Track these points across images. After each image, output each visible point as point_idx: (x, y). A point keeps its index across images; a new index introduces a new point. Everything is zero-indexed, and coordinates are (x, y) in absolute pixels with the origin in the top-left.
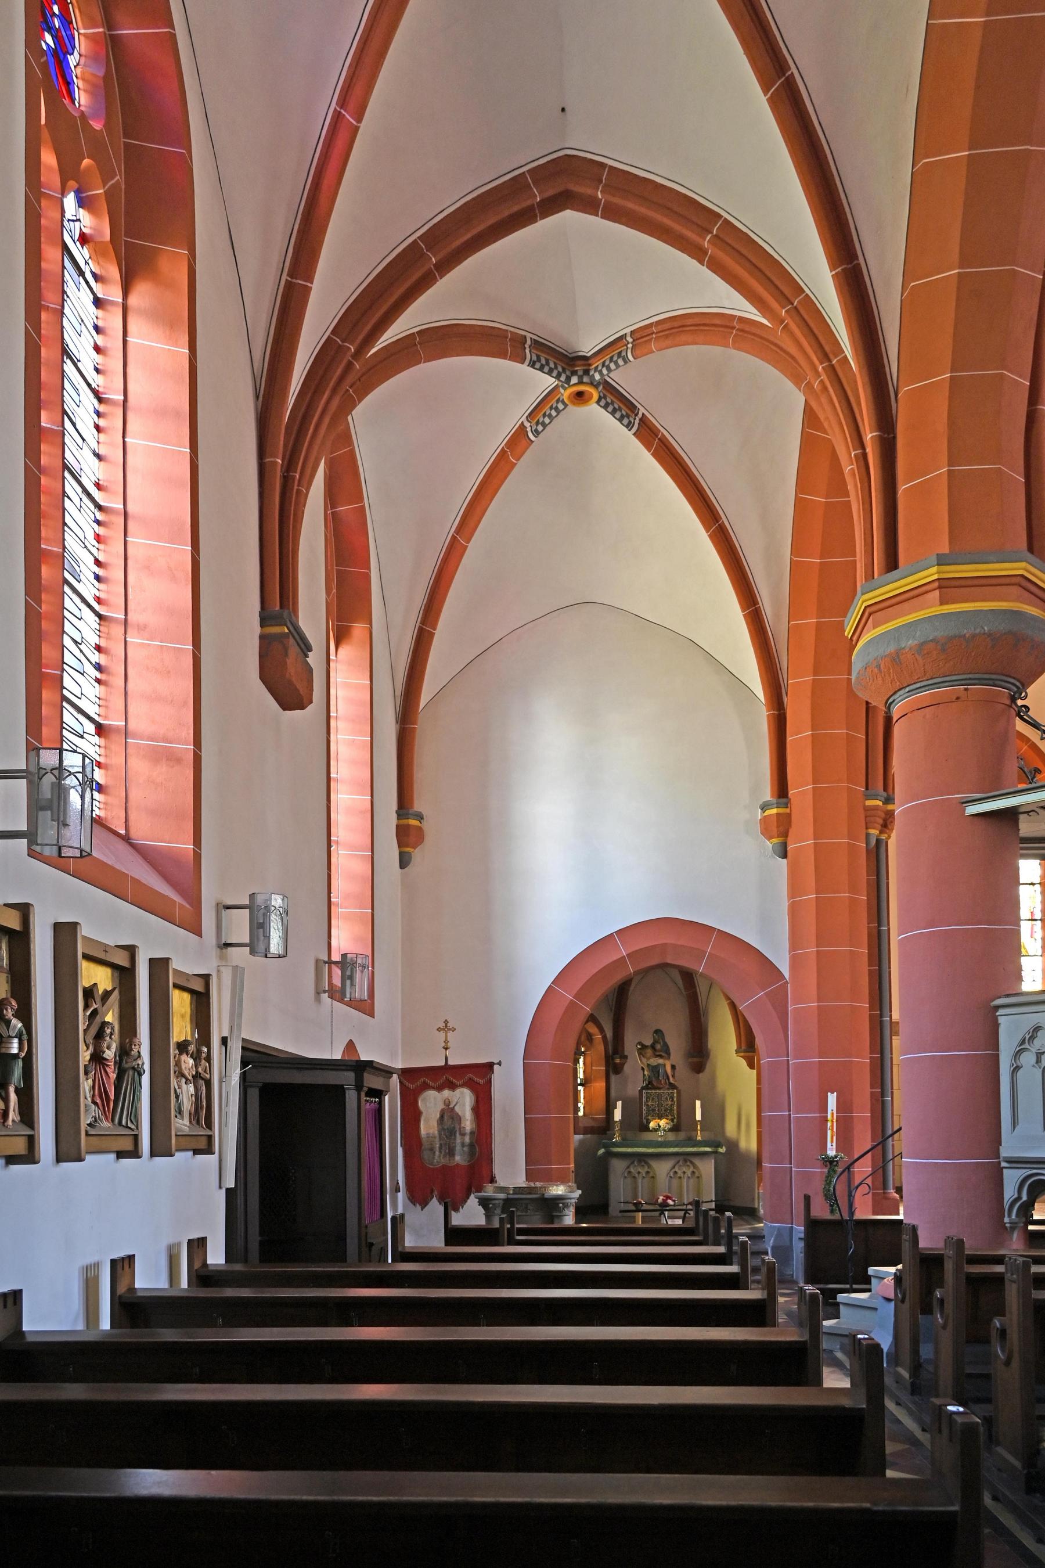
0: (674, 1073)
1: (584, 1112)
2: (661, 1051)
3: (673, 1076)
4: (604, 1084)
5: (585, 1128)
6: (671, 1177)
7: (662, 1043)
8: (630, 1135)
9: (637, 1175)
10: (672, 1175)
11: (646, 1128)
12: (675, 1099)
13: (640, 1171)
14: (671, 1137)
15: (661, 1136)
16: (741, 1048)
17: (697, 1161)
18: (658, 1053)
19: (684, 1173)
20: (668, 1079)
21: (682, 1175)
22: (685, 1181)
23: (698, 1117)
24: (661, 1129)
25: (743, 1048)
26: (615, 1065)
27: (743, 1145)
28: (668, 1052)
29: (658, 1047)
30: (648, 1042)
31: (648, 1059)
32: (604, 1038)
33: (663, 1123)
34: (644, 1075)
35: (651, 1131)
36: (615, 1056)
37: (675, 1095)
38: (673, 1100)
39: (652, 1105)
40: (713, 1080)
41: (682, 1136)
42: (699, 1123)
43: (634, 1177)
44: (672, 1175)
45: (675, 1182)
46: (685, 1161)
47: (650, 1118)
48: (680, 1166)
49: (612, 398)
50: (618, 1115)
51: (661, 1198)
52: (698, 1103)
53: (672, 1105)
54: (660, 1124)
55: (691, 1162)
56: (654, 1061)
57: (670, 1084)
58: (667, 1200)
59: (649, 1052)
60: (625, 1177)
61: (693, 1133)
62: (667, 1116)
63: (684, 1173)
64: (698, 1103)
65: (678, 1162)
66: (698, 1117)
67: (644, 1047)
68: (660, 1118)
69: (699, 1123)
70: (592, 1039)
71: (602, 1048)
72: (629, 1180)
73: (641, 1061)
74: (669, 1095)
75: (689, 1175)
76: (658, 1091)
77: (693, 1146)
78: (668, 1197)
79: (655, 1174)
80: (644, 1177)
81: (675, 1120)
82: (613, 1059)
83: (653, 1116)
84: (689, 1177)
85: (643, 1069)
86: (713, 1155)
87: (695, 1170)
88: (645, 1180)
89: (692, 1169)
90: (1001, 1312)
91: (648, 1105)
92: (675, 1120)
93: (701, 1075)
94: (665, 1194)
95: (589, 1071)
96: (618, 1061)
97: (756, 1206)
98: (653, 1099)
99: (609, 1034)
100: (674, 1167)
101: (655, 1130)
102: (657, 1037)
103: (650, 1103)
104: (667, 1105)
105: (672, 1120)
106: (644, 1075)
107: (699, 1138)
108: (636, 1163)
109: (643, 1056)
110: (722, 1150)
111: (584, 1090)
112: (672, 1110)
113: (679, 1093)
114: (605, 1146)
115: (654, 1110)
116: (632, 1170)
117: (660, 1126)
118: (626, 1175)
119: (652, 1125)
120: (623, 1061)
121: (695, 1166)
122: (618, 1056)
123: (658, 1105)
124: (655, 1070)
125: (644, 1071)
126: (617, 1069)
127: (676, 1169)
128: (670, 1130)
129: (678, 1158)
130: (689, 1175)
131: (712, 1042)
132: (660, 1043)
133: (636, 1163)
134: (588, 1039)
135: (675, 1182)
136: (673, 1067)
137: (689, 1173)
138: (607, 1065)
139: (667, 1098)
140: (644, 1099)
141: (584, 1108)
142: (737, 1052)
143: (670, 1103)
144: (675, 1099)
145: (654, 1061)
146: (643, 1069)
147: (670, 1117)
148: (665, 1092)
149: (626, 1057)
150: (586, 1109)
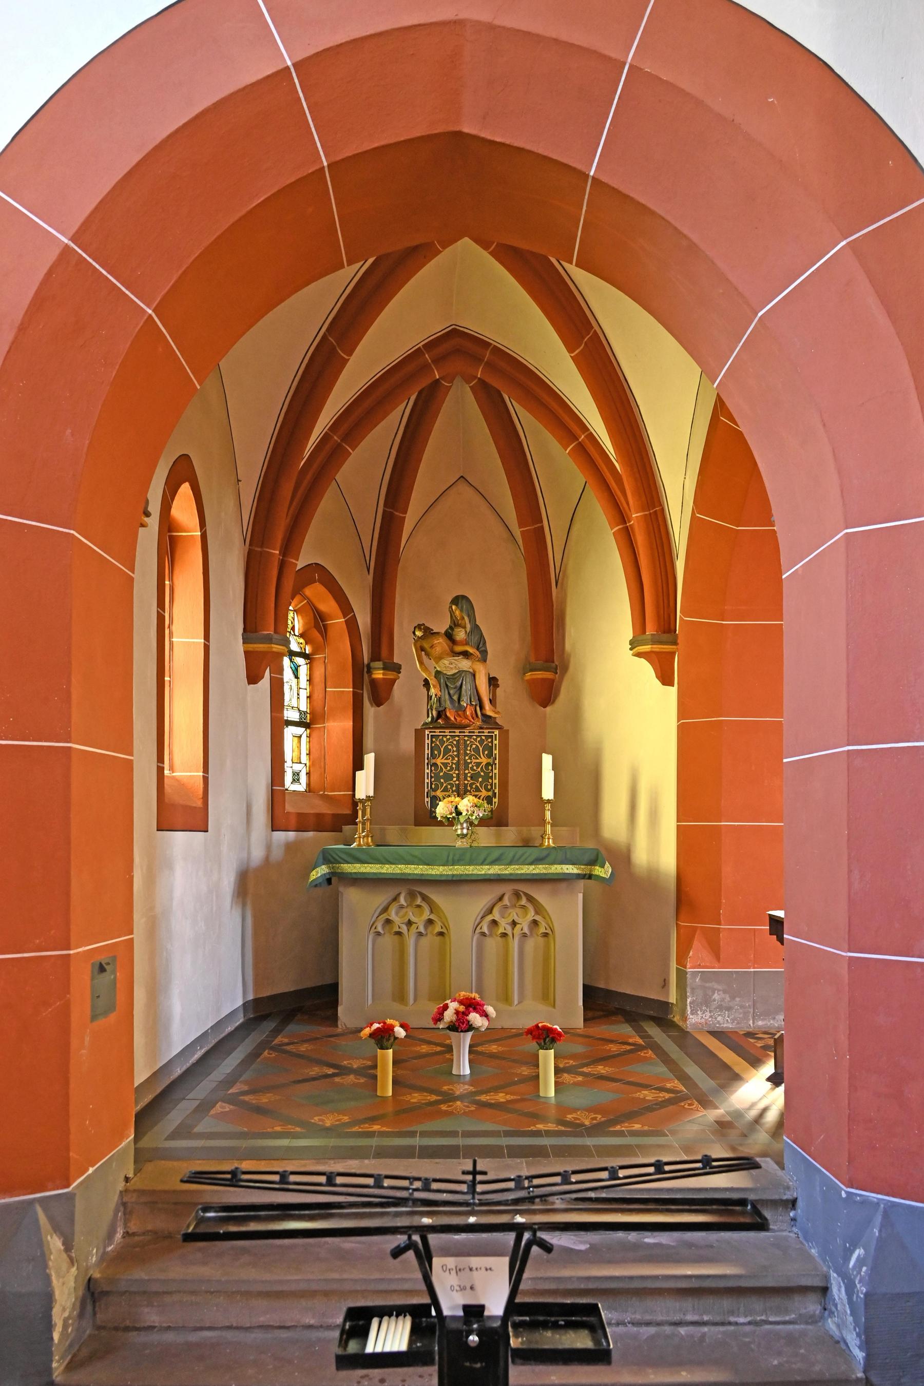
0: (494, 695)
1: (308, 785)
2: (467, 644)
3: (492, 701)
4: (349, 724)
5: (300, 815)
6: (483, 934)
7: (468, 627)
8: (393, 833)
9: (404, 929)
10: (485, 930)
11: (427, 818)
12: (496, 752)
13: (413, 919)
14: (485, 837)
15: (463, 836)
16: (644, 632)
17: (541, 895)
18: (459, 649)
19: (514, 924)
20: (482, 708)
21: (509, 930)
22: (515, 944)
23: (548, 792)
24: (462, 819)
25: (650, 630)
26: (373, 682)
27: (641, 856)
28: (481, 645)
29: (460, 635)
30: (441, 626)
31: (439, 659)
32: (352, 625)
33: (465, 804)
34: (430, 698)
35: (440, 824)
36: (374, 665)
37: (497, 742)
38: (490, 755)
39: (445, 765)
40: (575, 717)
41: (510, 835)
42: (548, 807)
43: (399, 934)
44: (485, 930)
45: (493, 944)
46: (412, 895)
47: (439, 793)
48: (506, 907)
49: (564, 1318)
50: (365, 785)
51: (453, 1006)
52: (547, 760)
53: (488, 764)
54: (461, 807)
55: (425, 898)
56: (451, 665)
57: (487, 718)
58: (466, 1014)
59: (440, 644)
60: (378, 934)
61: (535, 831)
62: (477, 790)
63: (514, 924)
64: (547, 760)
65: (396, 899)
66: (548, 792)
67: (429, 633)
68: (461, 795)
69: (548, 807)
70: (325, 626)
71: (345, 646)
72: (388, 941)
73: (421, 663)
74: (481, 742)
75: (526, 930)
76: (457, 732)
77: (537, 861)
78: (471, 1005)
79: (445, 925)
80: (420, 934)
81: (496, 800)
82: (369, 670)
83: (446, 790)
84: (524, 935)
85: (426, 684)
86: (582, 883)
87: (538, 918)
88: (424, 941)
89: (531, 915)
90: (767, 1024)
91: (435, 765)
92: (496, 800)
93: (548, 709)
94: (463, 994)
95: (318, 695)
96: (378, 675)
97: (673, 999)
98: (447, 751)
99: (364, 620)
100: (490, 911)
101: (450, 822)
102: (457, 613)
103: (439, 761)
104: (478, 764)
105: (489, 800)
106: (430, 698)
107: (549, 842)
108: (402, 900)
109: (427, 654)
110: (604, 871)
111: (309, 737)
112: (488, 777)
113: (505, 734)
114: (327, 858)
115: (448, 777)
116: (393, 914)
117: (459, 813)
118: (380, 929)
119: (442, 809)
120: (391, 675)
121: (539, 909)
122: (379, 664)
123: (458, 764)
124: (451, 682)
125: (428, 690)
126: (380, 695)
127: (496, 915)
128: (483, 822)
129: (498, 890)
130: (526, 930)
131: (575, 638)
132: (465, 627)
133: (402, 900)
134: (317, 626)
135: (493, 944)
136: (493, 682)
137: (524, 925)
138: (357, 683)
139: (477, 748)
140: (427, 751)
141: (308, 774)
142: (633, 644)
143: (484, 760)
144: (496, 752)
145: (451, 665)
146: (426, 684)
147: (484, 793)
148: (474, 735)
149: (397, 668)
150: (314, 777)
